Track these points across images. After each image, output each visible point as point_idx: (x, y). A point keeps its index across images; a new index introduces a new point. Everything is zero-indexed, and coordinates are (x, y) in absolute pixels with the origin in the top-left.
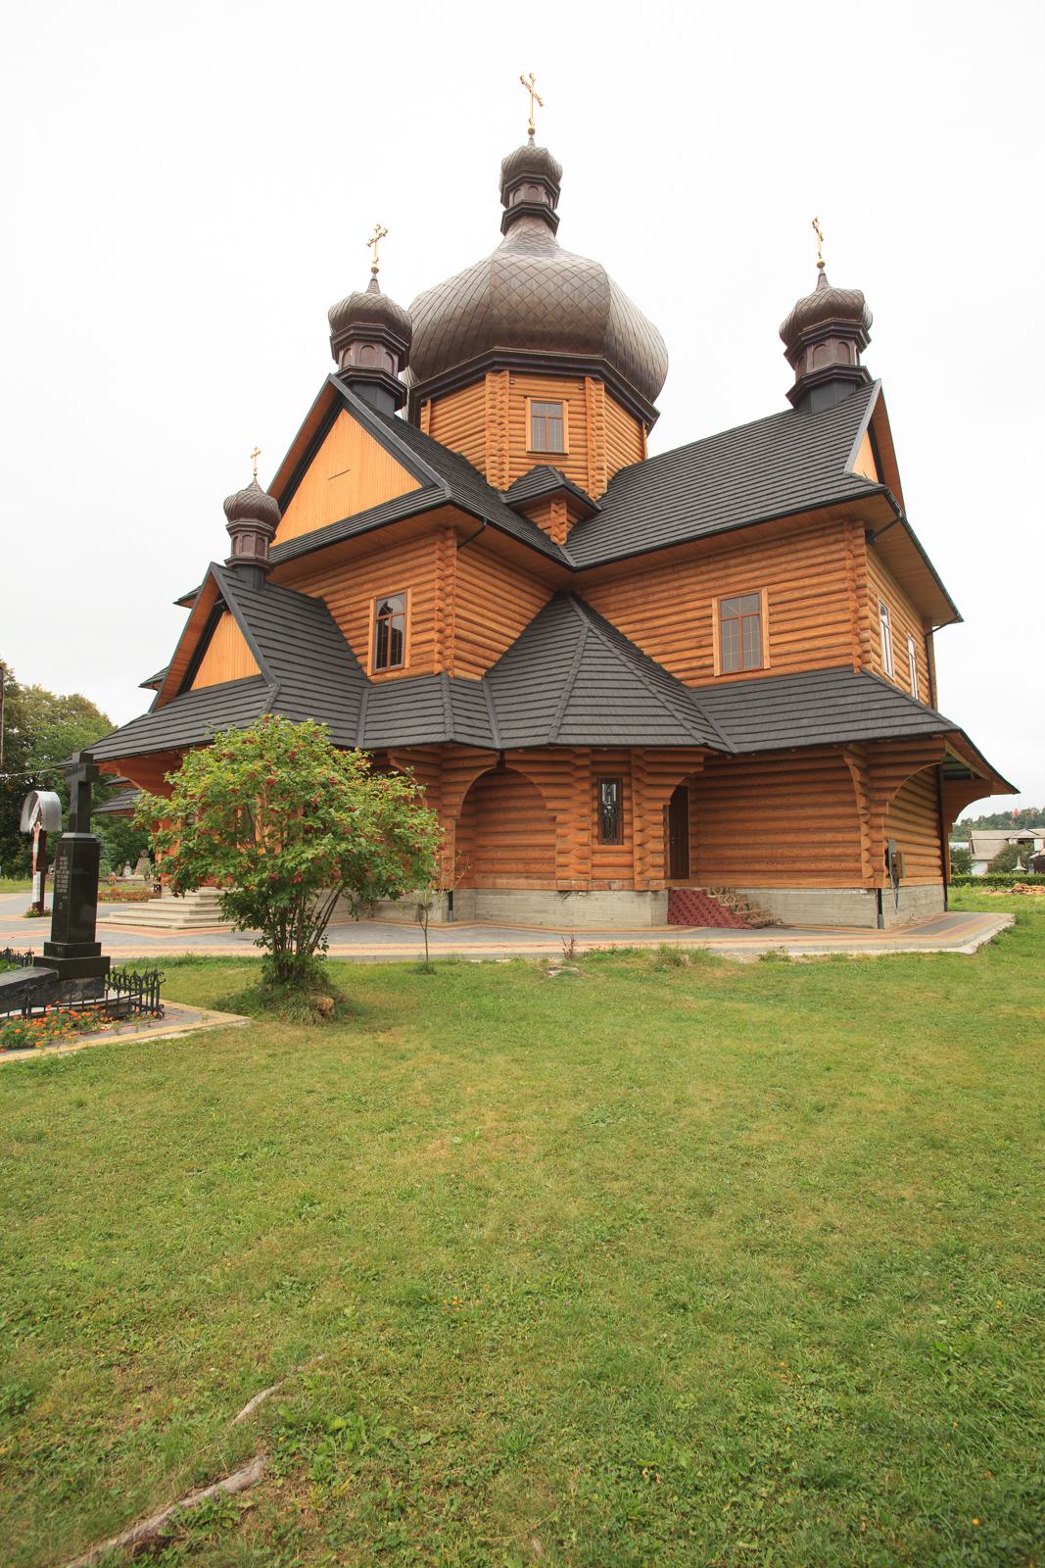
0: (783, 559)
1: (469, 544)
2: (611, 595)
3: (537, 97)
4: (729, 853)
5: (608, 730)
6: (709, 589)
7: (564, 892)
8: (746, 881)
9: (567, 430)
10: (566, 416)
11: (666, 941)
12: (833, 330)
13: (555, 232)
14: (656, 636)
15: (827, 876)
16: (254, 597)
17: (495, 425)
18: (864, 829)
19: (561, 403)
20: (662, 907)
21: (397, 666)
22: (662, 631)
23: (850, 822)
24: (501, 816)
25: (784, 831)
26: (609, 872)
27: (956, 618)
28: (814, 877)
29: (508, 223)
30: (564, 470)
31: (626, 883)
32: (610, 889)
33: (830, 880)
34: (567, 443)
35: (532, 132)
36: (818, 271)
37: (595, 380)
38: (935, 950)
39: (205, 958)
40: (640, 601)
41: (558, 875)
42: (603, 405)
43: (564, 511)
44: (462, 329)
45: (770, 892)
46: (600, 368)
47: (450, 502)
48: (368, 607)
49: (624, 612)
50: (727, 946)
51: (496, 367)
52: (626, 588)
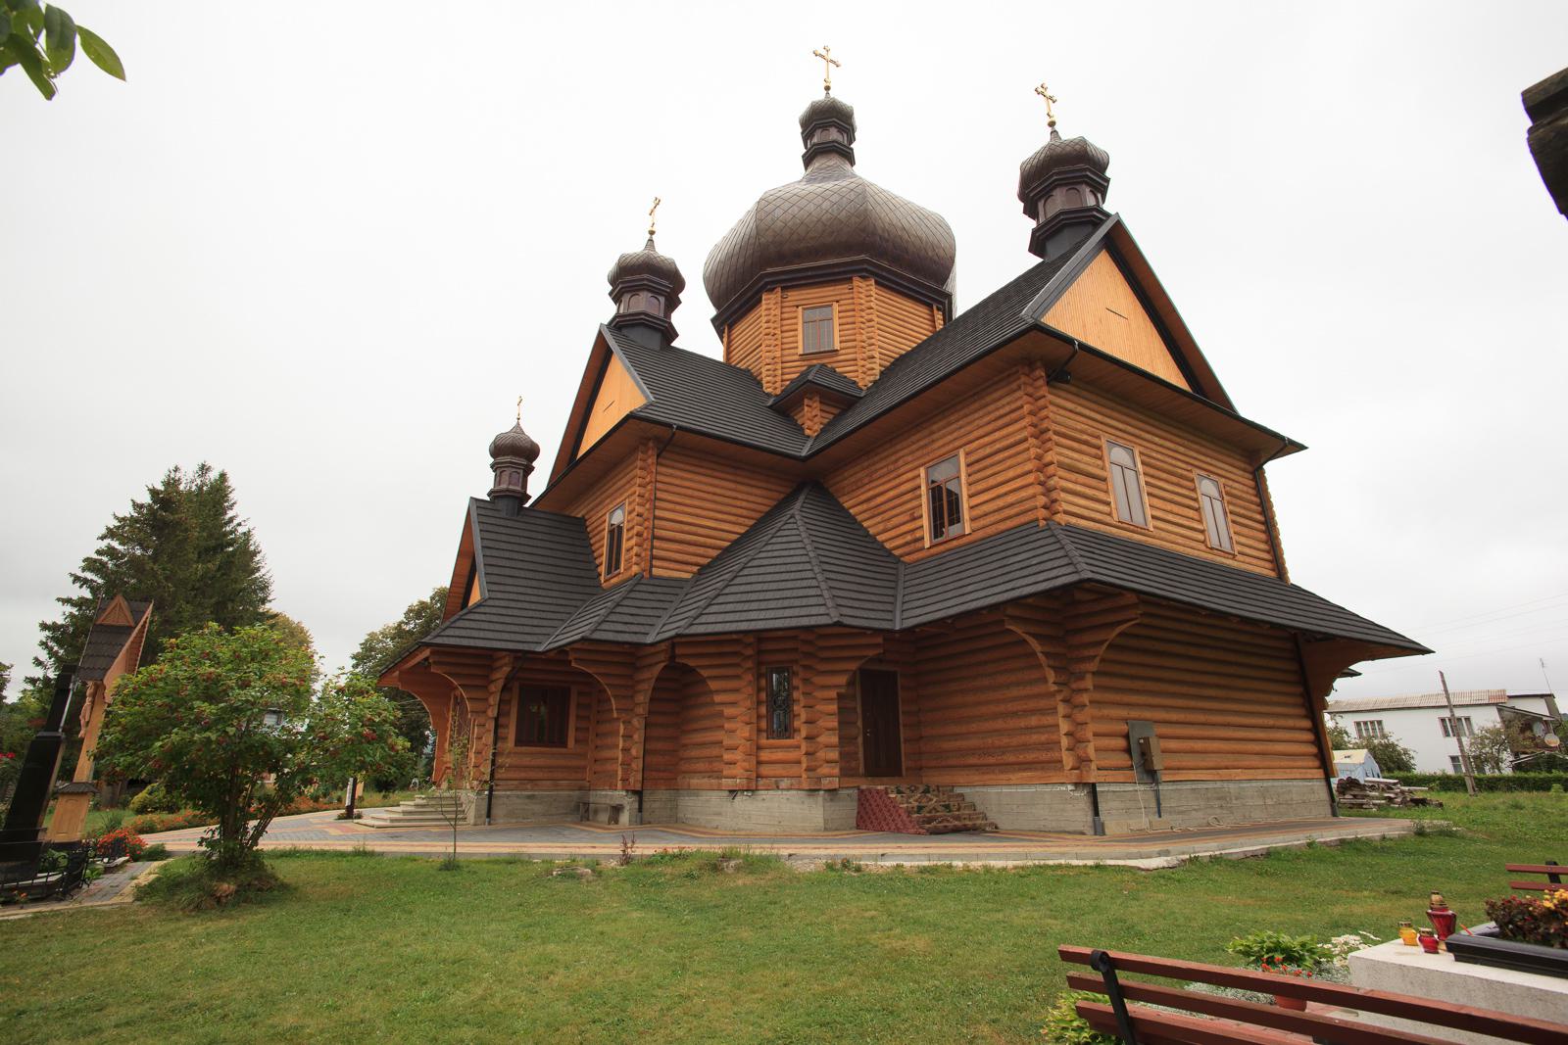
0: (976, 415)
1: (664, 454)
2: (846, 479)
3: (832, 61)
4: (947, 745)
5: (744, 616)
6: (918, 458)
7: (733, 792)
8: (961, 777)
9: (837, 328)
10: (836, 315)
11: (668, 846)
12: (1056, 180)
13: (852, 162)
14: (879, 514)
15: (1036, 769)
16: (510, 524)
17: (770, 337)
18: (1062, 709)
20: (847, 807)
22: (884, 507)
23: (1043, 703)
24: (702, 712)
25: (995, 716)
26: (778, 770)
27: (1286, 446)
28: (1025, 770)
29: (808, 160)
30: (834, 365)
31: (794, 781)
32: (778, 788)
33: (1038, 773)
34: (837, 339)
35: (827, 88)
36: (1050, 129)
37: (864, 278)
38: (1091, 863)
39: (308, 852)
40: (866, 481)
41: (725, 773)
42: (873, 299)
43: (816, 404)
44: (741, 260)
45: (984, 790)
46: (865, 266)
48: (970, 496)
49: (855, 494)
50: (856, 852)
51: (864, 274)
52: (856, 469)
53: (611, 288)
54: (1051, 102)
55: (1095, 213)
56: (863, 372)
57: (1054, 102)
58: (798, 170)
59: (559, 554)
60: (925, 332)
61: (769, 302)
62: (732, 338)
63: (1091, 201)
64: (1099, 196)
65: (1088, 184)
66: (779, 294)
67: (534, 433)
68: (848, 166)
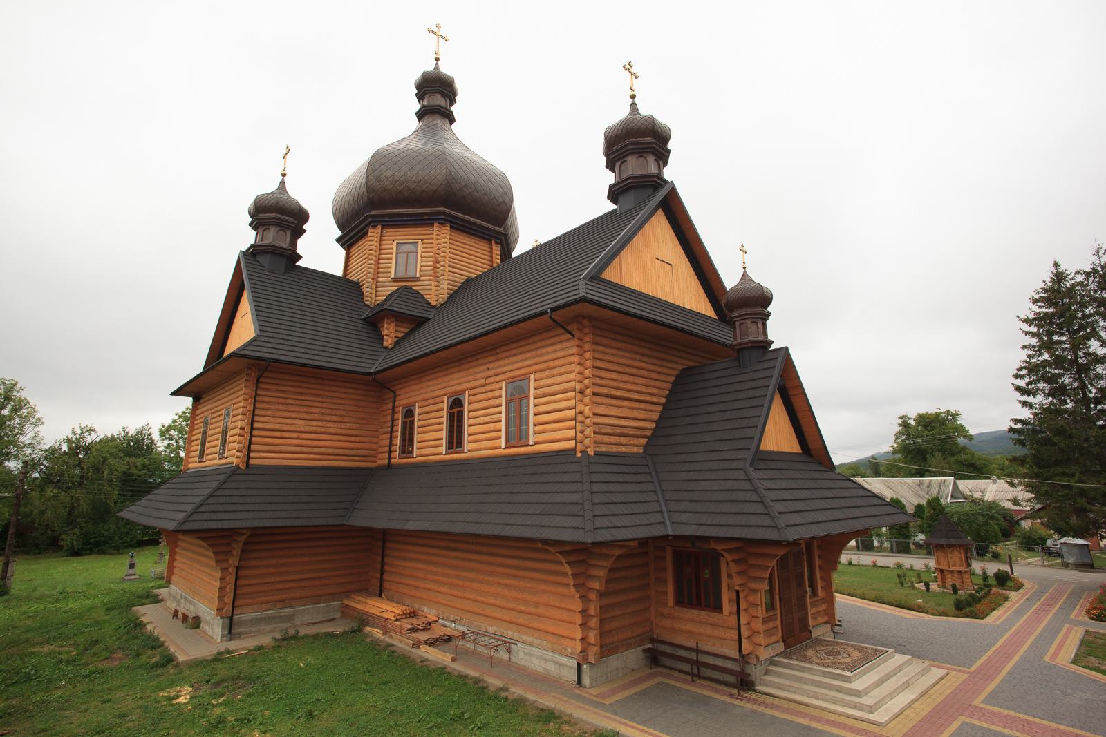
3: (442, 37)
19: (417, 243)
21: (459, 449)
29: (421, 115)
46: (370, 220)
47: (584, 300)
51: (373, 224)
53: (250, 219)
54: (634, 77)
55: (656, 179)
56: (435, 291)
57: (636, 78)
58: (414, 123)
59: (362, 338)
60: (485, 266)
61: (374, 234)
62: (351, 255)
63: (653, 169)
64: (661, 163)
65: (654, 154)
66: (379, 231)
67: (299, 193)
68: (448, 125)
